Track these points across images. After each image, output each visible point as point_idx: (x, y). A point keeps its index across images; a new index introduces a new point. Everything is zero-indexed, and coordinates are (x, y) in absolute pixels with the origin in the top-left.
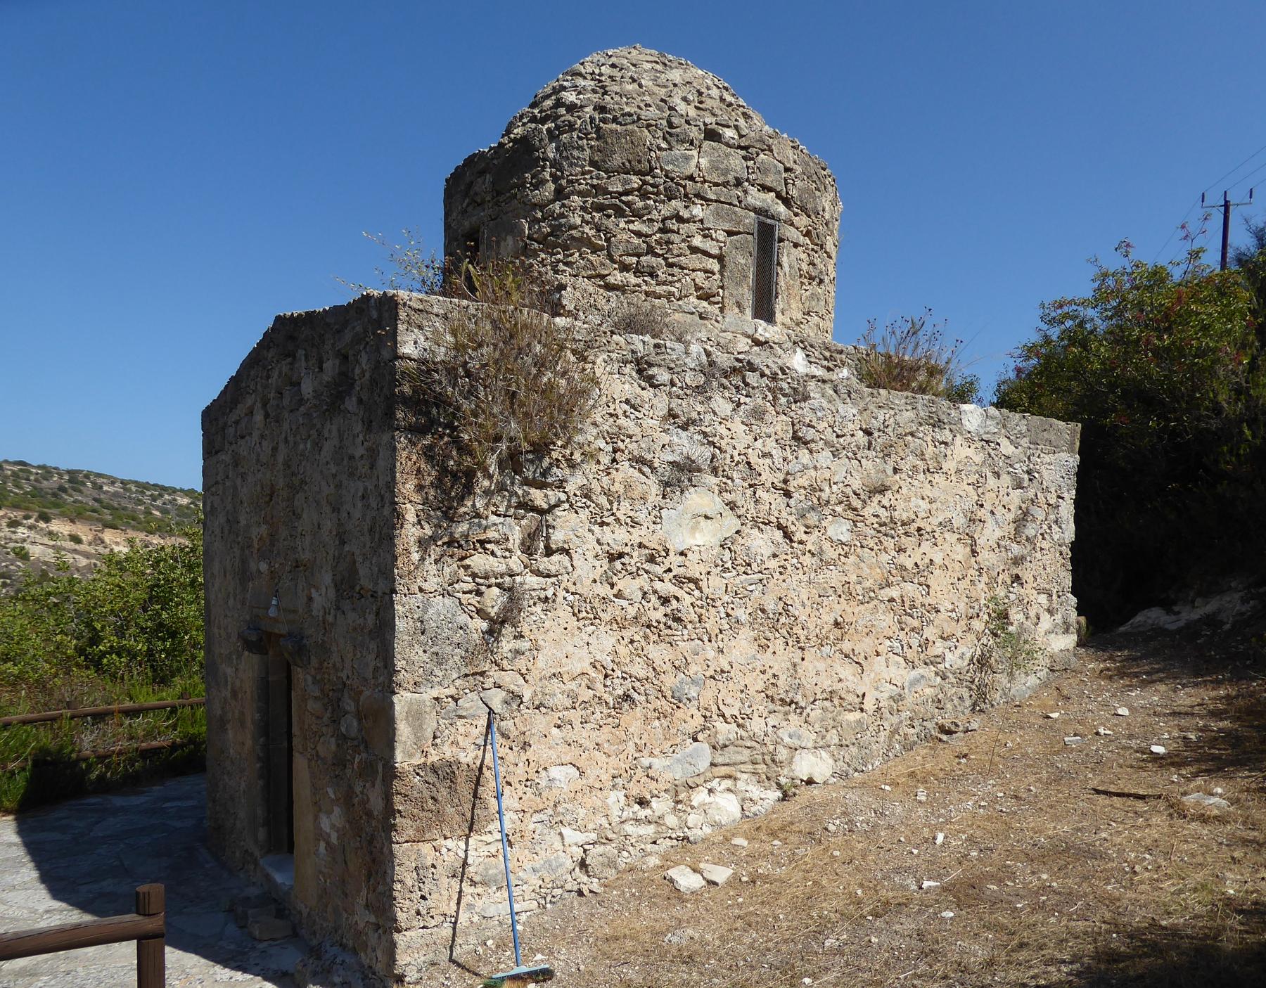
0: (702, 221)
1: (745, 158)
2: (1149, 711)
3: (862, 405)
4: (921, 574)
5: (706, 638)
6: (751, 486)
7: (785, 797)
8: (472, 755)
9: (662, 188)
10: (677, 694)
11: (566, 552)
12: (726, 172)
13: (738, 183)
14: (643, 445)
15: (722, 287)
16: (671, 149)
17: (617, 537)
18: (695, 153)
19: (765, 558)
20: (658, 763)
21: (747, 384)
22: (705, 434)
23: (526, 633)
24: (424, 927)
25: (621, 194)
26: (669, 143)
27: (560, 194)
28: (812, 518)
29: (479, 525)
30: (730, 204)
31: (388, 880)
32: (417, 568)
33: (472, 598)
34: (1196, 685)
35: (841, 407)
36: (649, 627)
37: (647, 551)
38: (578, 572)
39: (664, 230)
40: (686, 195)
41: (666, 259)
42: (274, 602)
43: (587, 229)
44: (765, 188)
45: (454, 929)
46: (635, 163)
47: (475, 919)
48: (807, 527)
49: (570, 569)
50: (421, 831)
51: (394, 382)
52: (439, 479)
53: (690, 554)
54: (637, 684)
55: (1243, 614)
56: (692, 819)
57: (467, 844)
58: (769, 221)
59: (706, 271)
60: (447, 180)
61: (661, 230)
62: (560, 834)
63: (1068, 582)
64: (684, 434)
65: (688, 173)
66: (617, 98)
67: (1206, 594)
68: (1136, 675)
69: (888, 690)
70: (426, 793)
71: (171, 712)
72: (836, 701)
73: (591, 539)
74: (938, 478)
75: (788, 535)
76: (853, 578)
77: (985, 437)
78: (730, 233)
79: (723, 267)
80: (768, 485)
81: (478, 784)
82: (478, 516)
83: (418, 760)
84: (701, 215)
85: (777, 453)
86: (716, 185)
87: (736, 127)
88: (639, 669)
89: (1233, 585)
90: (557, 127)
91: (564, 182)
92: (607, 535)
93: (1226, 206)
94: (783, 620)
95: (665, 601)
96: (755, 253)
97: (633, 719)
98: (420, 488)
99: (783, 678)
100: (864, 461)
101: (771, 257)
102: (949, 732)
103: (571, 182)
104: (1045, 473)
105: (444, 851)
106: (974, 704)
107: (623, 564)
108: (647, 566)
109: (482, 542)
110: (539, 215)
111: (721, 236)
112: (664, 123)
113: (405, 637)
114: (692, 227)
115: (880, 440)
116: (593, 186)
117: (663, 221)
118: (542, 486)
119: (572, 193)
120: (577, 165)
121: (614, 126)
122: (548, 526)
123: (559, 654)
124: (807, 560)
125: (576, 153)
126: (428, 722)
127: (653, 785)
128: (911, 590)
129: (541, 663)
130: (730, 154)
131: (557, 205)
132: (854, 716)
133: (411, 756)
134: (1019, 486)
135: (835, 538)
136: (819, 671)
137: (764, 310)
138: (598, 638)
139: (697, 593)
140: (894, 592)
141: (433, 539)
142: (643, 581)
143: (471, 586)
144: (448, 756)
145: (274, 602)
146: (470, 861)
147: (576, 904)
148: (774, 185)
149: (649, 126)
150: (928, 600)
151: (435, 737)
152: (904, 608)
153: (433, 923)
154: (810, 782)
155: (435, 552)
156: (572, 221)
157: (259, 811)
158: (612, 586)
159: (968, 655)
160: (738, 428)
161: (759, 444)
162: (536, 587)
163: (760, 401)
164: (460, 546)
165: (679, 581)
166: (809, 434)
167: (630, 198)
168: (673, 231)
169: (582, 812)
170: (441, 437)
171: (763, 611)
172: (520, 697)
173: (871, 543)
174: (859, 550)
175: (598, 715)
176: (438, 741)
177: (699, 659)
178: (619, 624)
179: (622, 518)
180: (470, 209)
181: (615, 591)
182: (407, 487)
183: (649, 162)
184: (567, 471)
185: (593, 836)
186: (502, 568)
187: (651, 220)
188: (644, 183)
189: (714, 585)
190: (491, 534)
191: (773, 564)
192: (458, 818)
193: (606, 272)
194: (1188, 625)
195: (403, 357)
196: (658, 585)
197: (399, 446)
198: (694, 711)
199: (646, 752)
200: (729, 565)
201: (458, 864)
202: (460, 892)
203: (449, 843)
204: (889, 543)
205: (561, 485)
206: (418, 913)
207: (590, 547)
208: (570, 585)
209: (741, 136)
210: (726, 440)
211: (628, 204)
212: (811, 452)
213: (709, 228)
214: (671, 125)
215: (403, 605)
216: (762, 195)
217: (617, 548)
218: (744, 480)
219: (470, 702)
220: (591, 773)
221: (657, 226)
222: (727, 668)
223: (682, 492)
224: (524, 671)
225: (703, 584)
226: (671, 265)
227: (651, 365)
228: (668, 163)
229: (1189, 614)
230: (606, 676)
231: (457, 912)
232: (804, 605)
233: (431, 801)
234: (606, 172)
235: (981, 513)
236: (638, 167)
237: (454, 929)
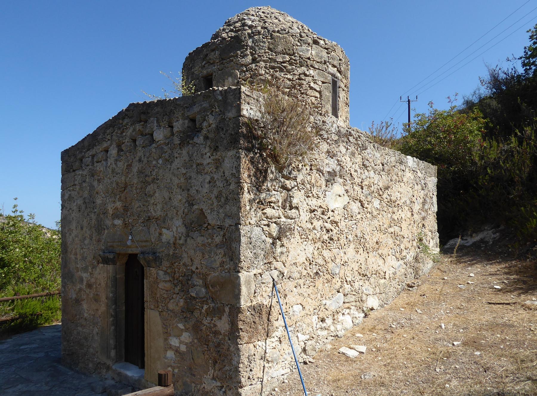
0: (313, 77)
1: (327, 53)
2: (479, 276)
4: (397, 222)
6: (352, 183)
7: (366, 316)
8: (268, 301)
9: (298, 61)
11: (297, 208)
13: (325, 63)
18: (310, 48)
20: (328, 302)
22: (338, 160)
23: (285, 244)
25: (282, 63)
27: (254, 60)
28: (369, 198)
29: (270, 195)
31: (234, 363)
32: (248, 213)
33: (266, 228)
34: (491, 264)
36: (323, 243)
37: (322, 209)
38: (301, 217)
40: (307, 66)
42: (130, 238)
43: (267, 76)
44: (334, 66)
45: (262, 384)
46: (287, 50)
47: (269, 379)
50: (250, 338)
51: (239, 127)
52: (255, 173)
54: (320, 268)
55: (495, 238)
56: (339, 327)
57: (266, 343)
58: (335, 79)
60: (190, 54)
62: (297, 336)
63: (436, 228)
64: (332, 160)
65: (308, 57)
66: (271, 25)
67: (477, 231)
68: (465, 262)
69: (392, 270)
71: (11, 303)
72: (378, 274)
74: (402, 184)
75: (362, 205)
76: (381, 224)
77: (414, 169)
78: (323, 83)
79: (321, 96)
80: (357, 183)
81: (269, 314)
82: (269, 190)
83: (249, 304)
84: (313, 74)
85: (359, 170)
86: (318, 62)
87: (324, 40)
88: (320, 261)
89: (486, 228)
90: (252, 33)
91: (256, 56)
92: (309, 201)
93: (409, 101)
94: (362, 240)
95: (328, 231)
96: (331, 91)
97: (319, 283)
98: (249, 176)
99: (363, 265)
101: (336, 94)
102: (412, 287)
103: (260, 56)
104: (429, 184)
105: (258, 347)
106: (415, 276)
107: (315, 215)
108: (322, 216)
110: (245, 69)
111: (320, 83)
112: (298, 35)
113: (245, 246)
114: (311, 79)
115: (386, 167)
116: (269, 58)
117: (299, 75)
118: (288, 178)
119: (261, 61)
120: (262, 49)
121: (278, 34)
122: (290, 197)
124: (368, 215)
125: (262, 44)
126: (253, 287)
127: (327, 312)
128: (397, 229)
129: (290, 258)
131: (254, 65)
132: (383, 281)
133: (247, 302)
134: (423, 189)
136: (374, 262)
139: (337, 228)
140: (391, 230)
141: (254, 200)
142: (321, 222)
143: (266, 223)
144: (259, 302)
145: (130, 238)
146: (267, 351)
147: (305, 368)
148: (336, 65)
149: (292, 36)
150: (402, 233)
151: (255, 293)
152: (395, 236)
155: (255, 205)
156: (260, 72)
157: (112, 342)
158: (312, 224)
159: (413, 256)
164: (262, 204)
167: (285, 64)
168: (303, 80)
169: (304, 325)
170: (256, 153)
172: (283, 274)
173: (385, 209)
175: (308, 282)
176: (256, 294)
178: (314, 241)
179: (315, 194)
180: (206, 65)
181: (313, 226)
182: (245, 175)
184: (297, 173)
185: (308, 337)
186: (277, 215)
187: (295, 74)
188: (291, 59)
189: (342, 225)
190: (273, 199)
191: (359, 216)
192: (263, 331)
194: (474, 244)
197: (242, 156)
199: (324, 298)
201: (263, 353)
202: (264, 367)
203: (259, 343)
204: (391, 210)
205: (295, 179)
206: (249, 378)
209: (326, 44)
211: (285, 67)
214: (301, 36)
215: (244, 230)
216: (332, 68)
217: (313, 208)
219: (267, 277)
220: (307, 308)
221: (297, 77)
223: (332, 185)
224: (284, 262)
225: (339, 224)
228: (301, 51)
229: (477, 238)
230: (310, 264)
231: (263, 376)
233: (253, 323)
234: (275, 53)
235: (414, 199)
236: (289, 52)
237: (262, 384)
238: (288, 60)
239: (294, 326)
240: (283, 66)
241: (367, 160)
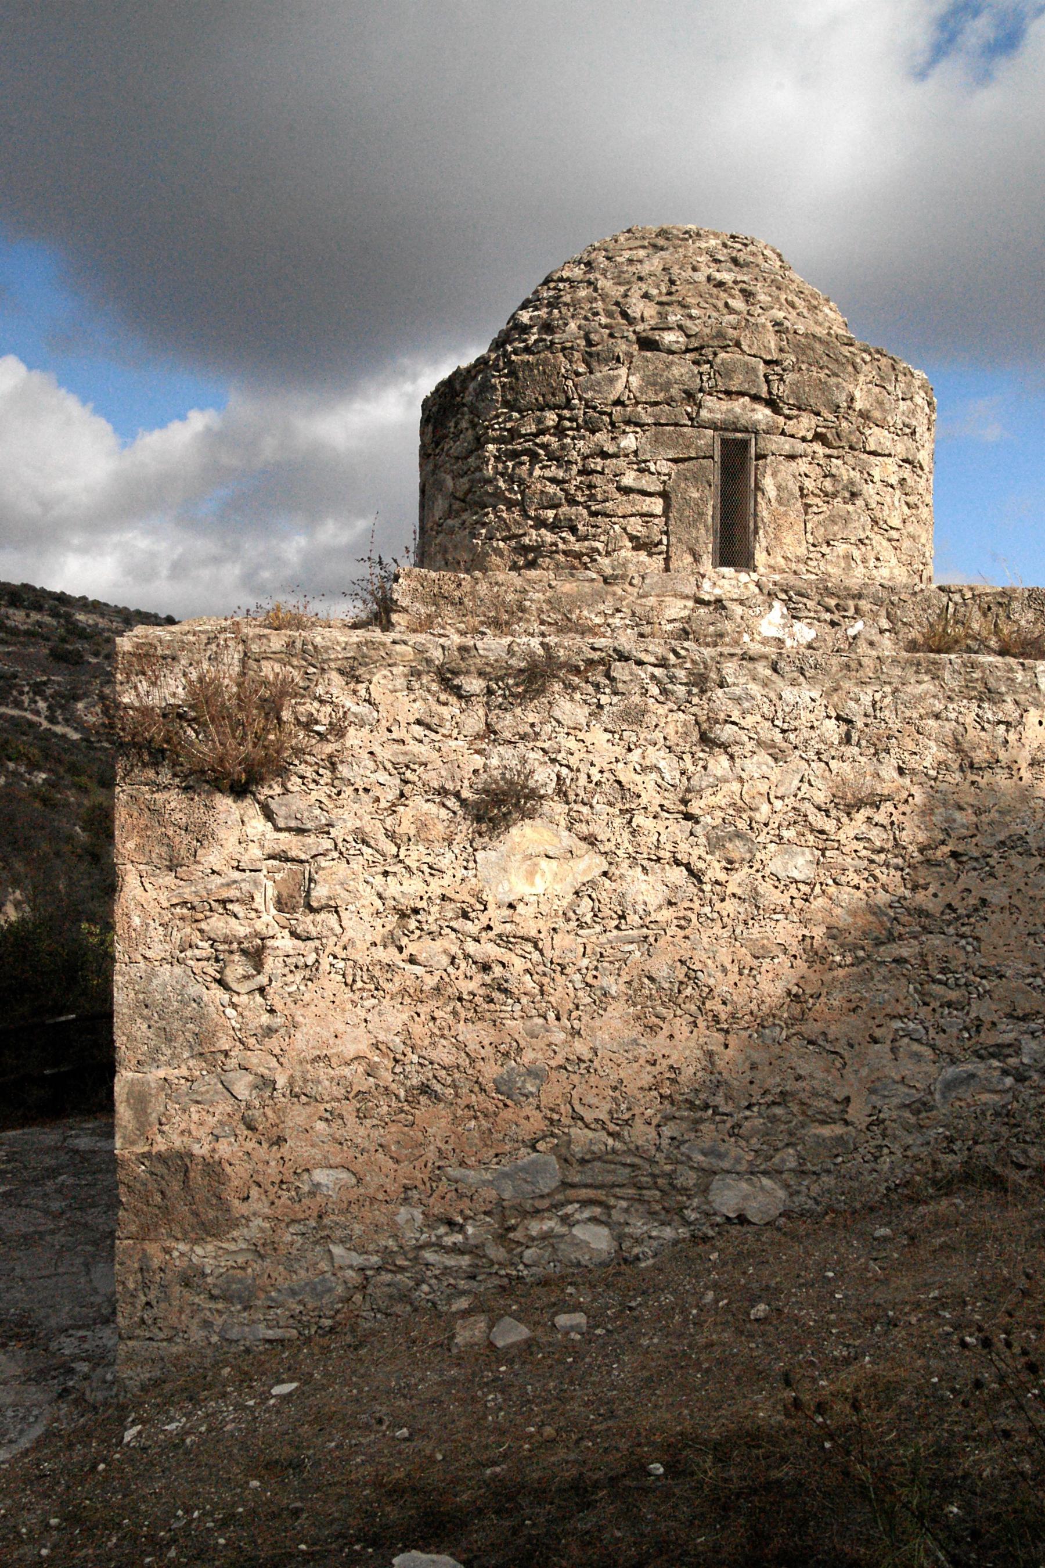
1: (696, 363)
3: (828, 684)
5: (551, 1015)
8: (207, 1147)
10: (504, 1088)
12: (667, 386)
14: (444, 773)
15: (666, 533)
16: (591, 372)
17: (408, 889)
19: (651, 908)
21: (612, 679)
24: (151, 1339)
26: (588, 365)
30: (676, 425)
35: (789, 694)
38: (350, 934)
39: (584, 472)
40: (612, 424)
41: (588, 507)
48: (731, 862)
49: (338, 930)
53: (520, 907)
58: (739, 435)
59: (642, 515)
61: (580, 473)
70: (152, 1186)
73: (368, 895)
75: (695, 875)
83: (141, 1148)
100: (833, 764)
105: (176, 1254)
107: (419, 922)
109: (223, 902)
111: (664, 467)
114: (622, 462)
123: (325, 1034)
130: (672, 363)
135: (782, 875)
137: (734, 551)
138: (380, 1014)
139: (536, 956)
142: (450, 943)
144: (178, 1144)
153: (162, 1336)
154: (742, 1219)
158: (400, 949)
160: (598, 736)
161: (635, 756)
162: (292, 952)
163: (636, 699)
165: (504, 940)
166: (726, 733)
168: (594, 472)
171: (651, 978)
172: (274, 1082)
174: (832, 890)
177: (540, 1044)
183: (565, 392)
185: (375, 1259)
193: (521, 532)
195: (126, 707)
196: (471, 947)
198: (530, 1110)
200: (588, 918)
207: (367, 903)
208: (338, 950)
210: (577, 756)
211: (545, 446)
212: (732, 757)
213: (642, 465)
216: (725, 405)
217: (406, 903)
218: (611, 805)
222: (587, 1055)
224: (277, 1051)
226: (594, 514)
227: (456, 673)
232: (725, 971)
238: (551, 423)
239: (313, 1223)
240: (537, 445)
241: (623, 657)
